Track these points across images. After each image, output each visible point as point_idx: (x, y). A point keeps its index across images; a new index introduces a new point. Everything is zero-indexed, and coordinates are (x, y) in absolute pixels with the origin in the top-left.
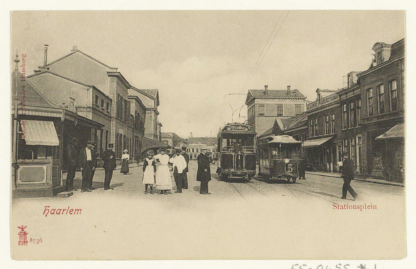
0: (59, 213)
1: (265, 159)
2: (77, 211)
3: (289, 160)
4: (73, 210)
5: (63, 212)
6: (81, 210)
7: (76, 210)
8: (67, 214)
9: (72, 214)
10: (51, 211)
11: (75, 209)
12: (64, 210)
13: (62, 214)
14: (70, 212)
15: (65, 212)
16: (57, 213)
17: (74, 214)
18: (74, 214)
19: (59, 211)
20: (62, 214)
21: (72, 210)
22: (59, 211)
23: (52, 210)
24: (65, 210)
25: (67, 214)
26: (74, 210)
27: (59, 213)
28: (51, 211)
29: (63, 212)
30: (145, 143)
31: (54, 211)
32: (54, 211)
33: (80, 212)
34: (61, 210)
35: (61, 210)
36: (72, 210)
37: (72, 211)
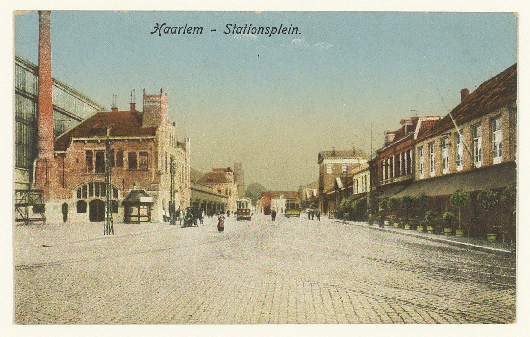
0: (175, 33)
1: (493, 136)
2: (197, 29)
3: (460, 134)
4: (287, 28)
5: (180, 30)
6: (297, 28)
7: (195, 28)
8: (184, 33)
9: (285, 33)
10: (276, 32)
11: (273, 28)
12: (180, 28)
13: (179, 33)
14: (188, 31)
15: (182, 30)
16: (252, 32)
17: (193, 33)
18: (193, 33)
19: (175, 29)
20: (179, 33)
21: (190, 29)
22: (175, 29)
23: (167, 27)
24: (183, 28)
25: (184, 33)
26: (193, 29)
27: (175, 33)
28: (276, 32)
29: (180, 30)
30: (185, 178)
31: (176, 30)
32: (176, 30)
33: (295, 32)
34: (177, 28)
35: (177, 28)
36: (190, 29)
37: (286, 30)
